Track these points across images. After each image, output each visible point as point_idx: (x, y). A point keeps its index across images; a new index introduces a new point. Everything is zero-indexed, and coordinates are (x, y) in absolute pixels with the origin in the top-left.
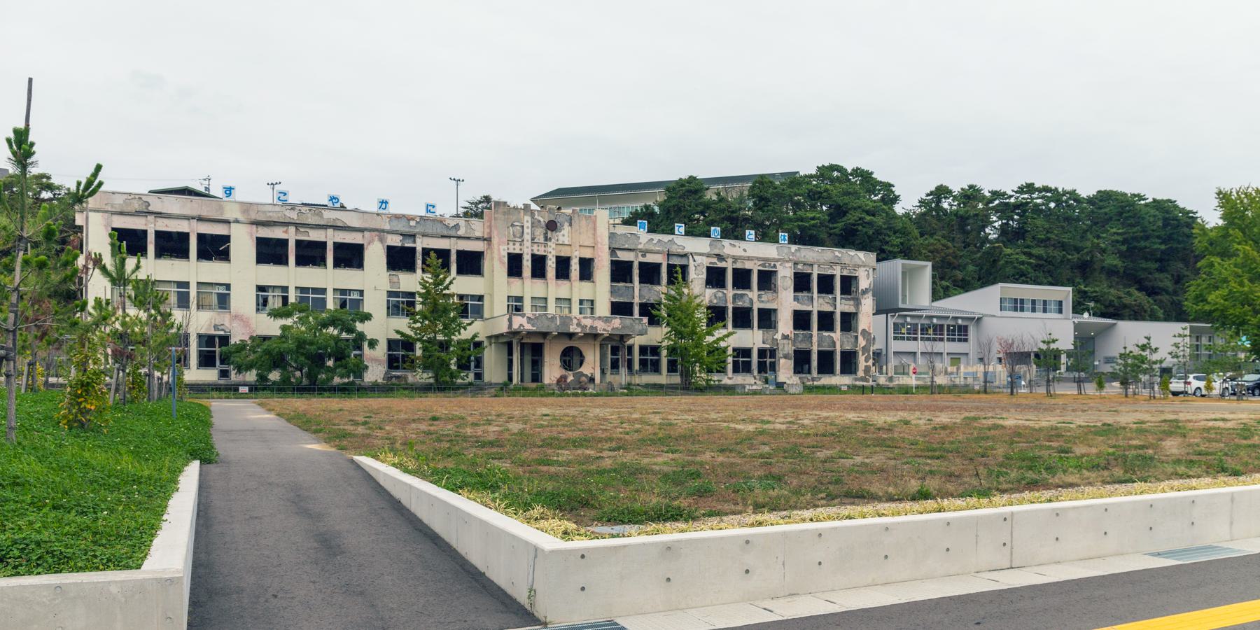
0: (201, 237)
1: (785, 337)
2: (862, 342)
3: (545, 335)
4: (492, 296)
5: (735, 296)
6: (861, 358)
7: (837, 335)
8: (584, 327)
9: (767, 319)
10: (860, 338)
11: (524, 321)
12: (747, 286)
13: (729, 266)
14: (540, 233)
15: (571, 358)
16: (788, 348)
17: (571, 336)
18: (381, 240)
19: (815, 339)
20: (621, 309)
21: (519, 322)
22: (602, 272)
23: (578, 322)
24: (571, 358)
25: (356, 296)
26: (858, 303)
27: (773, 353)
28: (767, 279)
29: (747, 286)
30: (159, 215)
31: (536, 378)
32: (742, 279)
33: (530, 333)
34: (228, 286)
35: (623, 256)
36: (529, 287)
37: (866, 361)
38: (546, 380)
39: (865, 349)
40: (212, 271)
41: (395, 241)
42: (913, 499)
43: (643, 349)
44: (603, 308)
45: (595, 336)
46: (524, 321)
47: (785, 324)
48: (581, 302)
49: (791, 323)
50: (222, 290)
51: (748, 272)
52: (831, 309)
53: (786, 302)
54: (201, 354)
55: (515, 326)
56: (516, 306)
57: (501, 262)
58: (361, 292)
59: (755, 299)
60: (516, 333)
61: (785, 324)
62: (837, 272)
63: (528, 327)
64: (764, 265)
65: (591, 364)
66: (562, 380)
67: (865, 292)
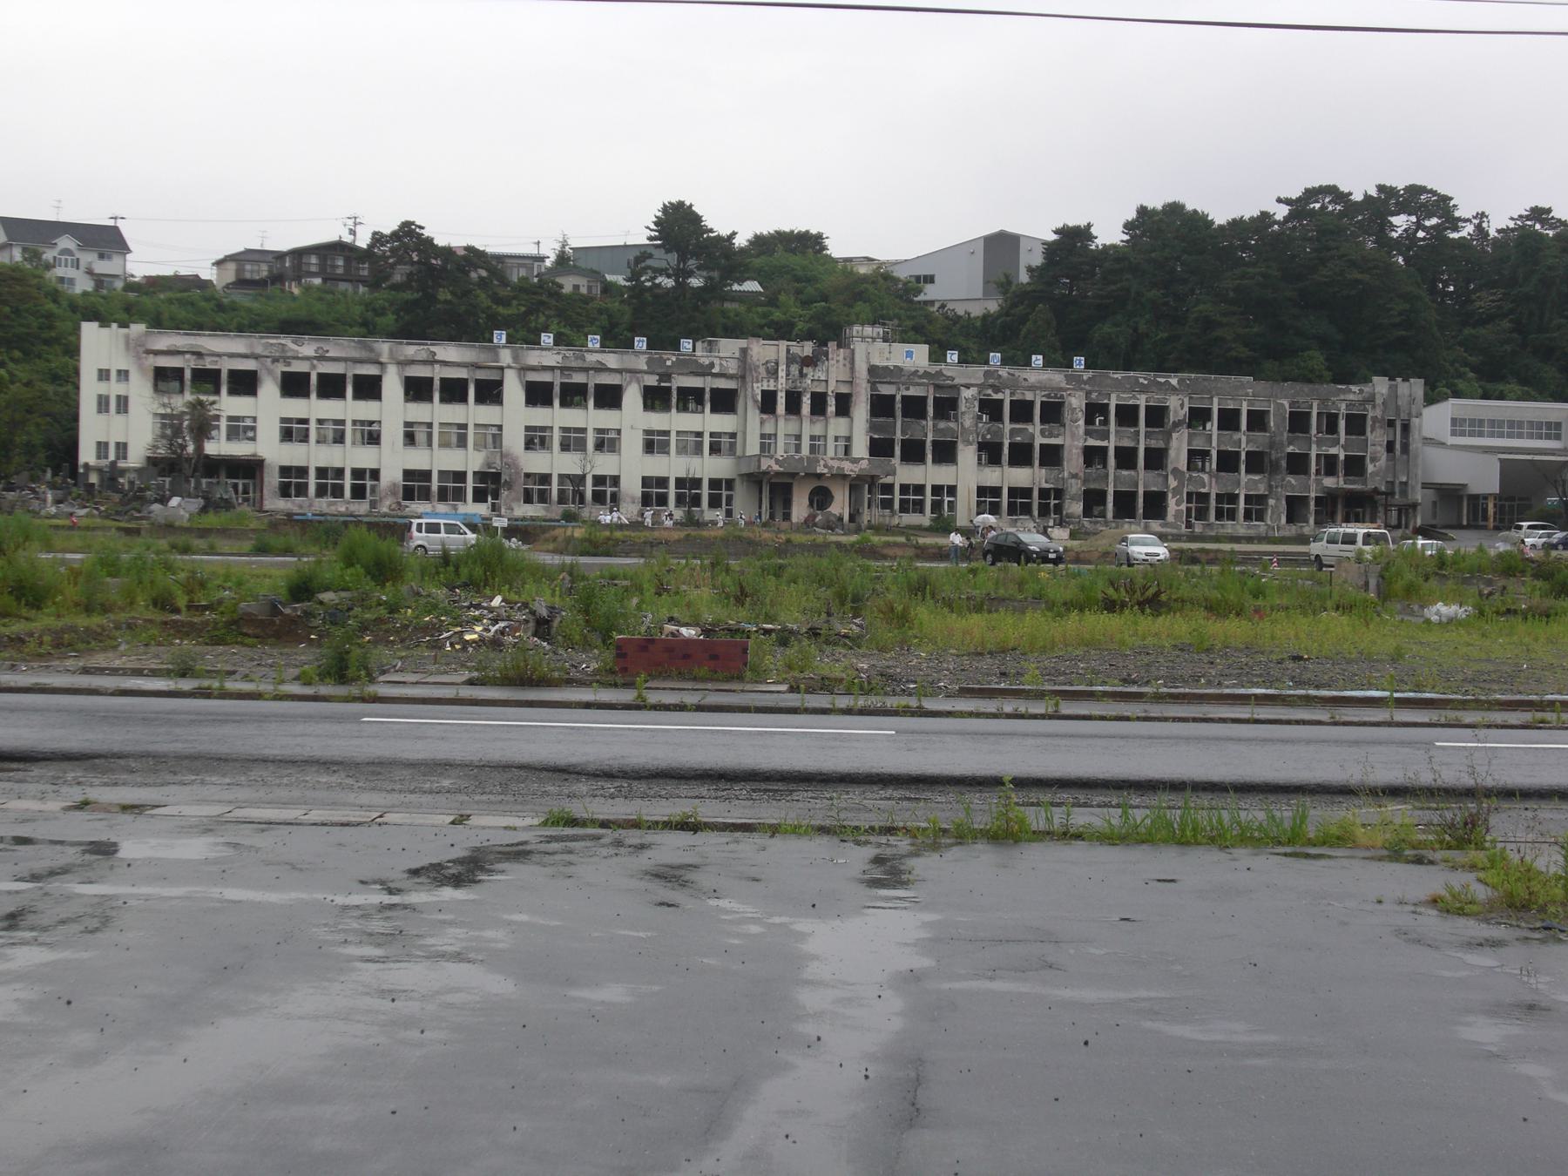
0: (478, 383)
1: (1075, 476)
2: (1173, 483)
3: (794, 475)
4: (745, 433)
5: (1012, 432)
6: (1172, 503)
7: (1245, 448)
8: (830, 468)
9: (1052, 456)
10: (1171, 478)
11: (772, 463)
12: (1028, 418)
13: (1006, 397)
14: (795, 369)
15: (821, 498)
16: (1075, 487)
17: (820, 476)
18: (638, 382)
19: (1111, 478)
20: (880, 448)
21: (766, 464)
22: (861, 410)
23: (830, 460)
24: (821, 498)
25: (613, 435)
26: (1168, 437)
27: (1059, 493)
28: (1053, 412)
29: (1028, 418)
30: (445, 363)
31: (787, 517)
32: (1022, 411)
33: (778, 474)
34: (500, 427)
35: (886, 390)
36: (784, 426)
37: (1178, 504)
38: (794, 519)
39: (1176, 491)
40: (485, 414)
41: (652, 381)
42: (978, 609)
43: (905, 489)
44: (861, 448)
45: (845, 476)
46: (772, 463)
47: (1073, 461)
48: (836, 439)
49: (1081, 460)
50: (494, 431)
51: (1030, 405)
52: (1132, 444)
53: (1073, 438)
54: (475, 490)
55: (764, 467)
56: (767, 441)
57: (756, 401)
58: (619, 432)
59: (1037, 433)
60: (765, 473)
61: (1073, 461)
62: (1142, 401)
63: (776, 468)
64: (1048, 396)
65: (840, 505)
66: (812, 517)
67: (1177, 425)
